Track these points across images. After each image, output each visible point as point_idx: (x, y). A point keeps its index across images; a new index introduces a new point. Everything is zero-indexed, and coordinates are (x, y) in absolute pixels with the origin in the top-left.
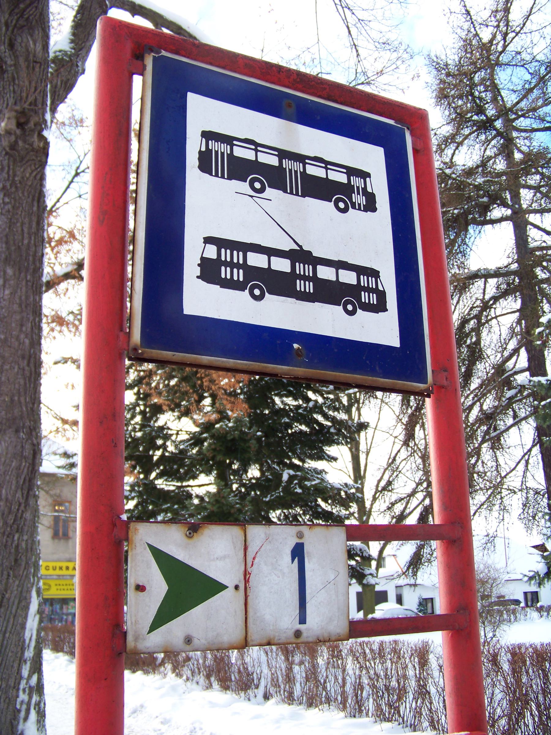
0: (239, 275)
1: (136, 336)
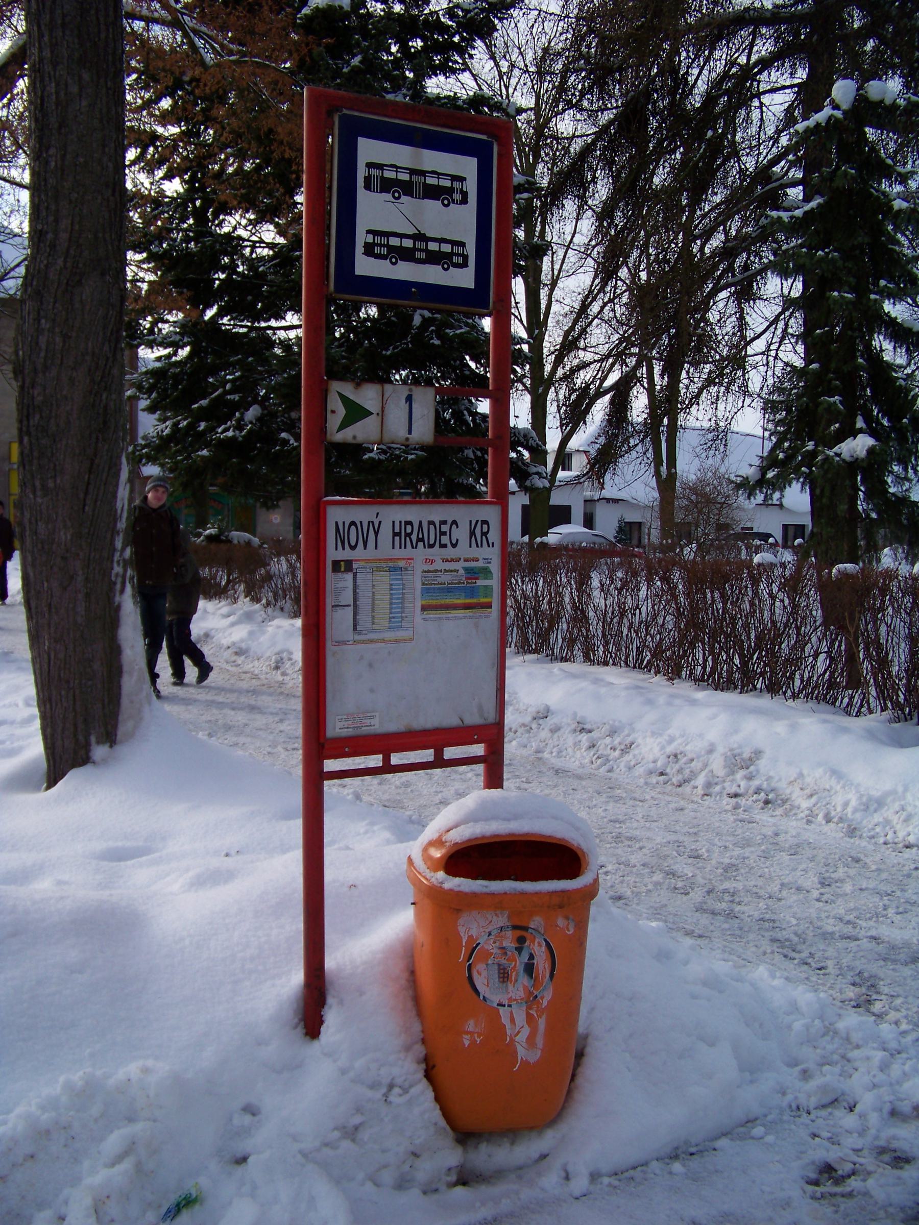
0: (384, 251)
1: (332, 287)
